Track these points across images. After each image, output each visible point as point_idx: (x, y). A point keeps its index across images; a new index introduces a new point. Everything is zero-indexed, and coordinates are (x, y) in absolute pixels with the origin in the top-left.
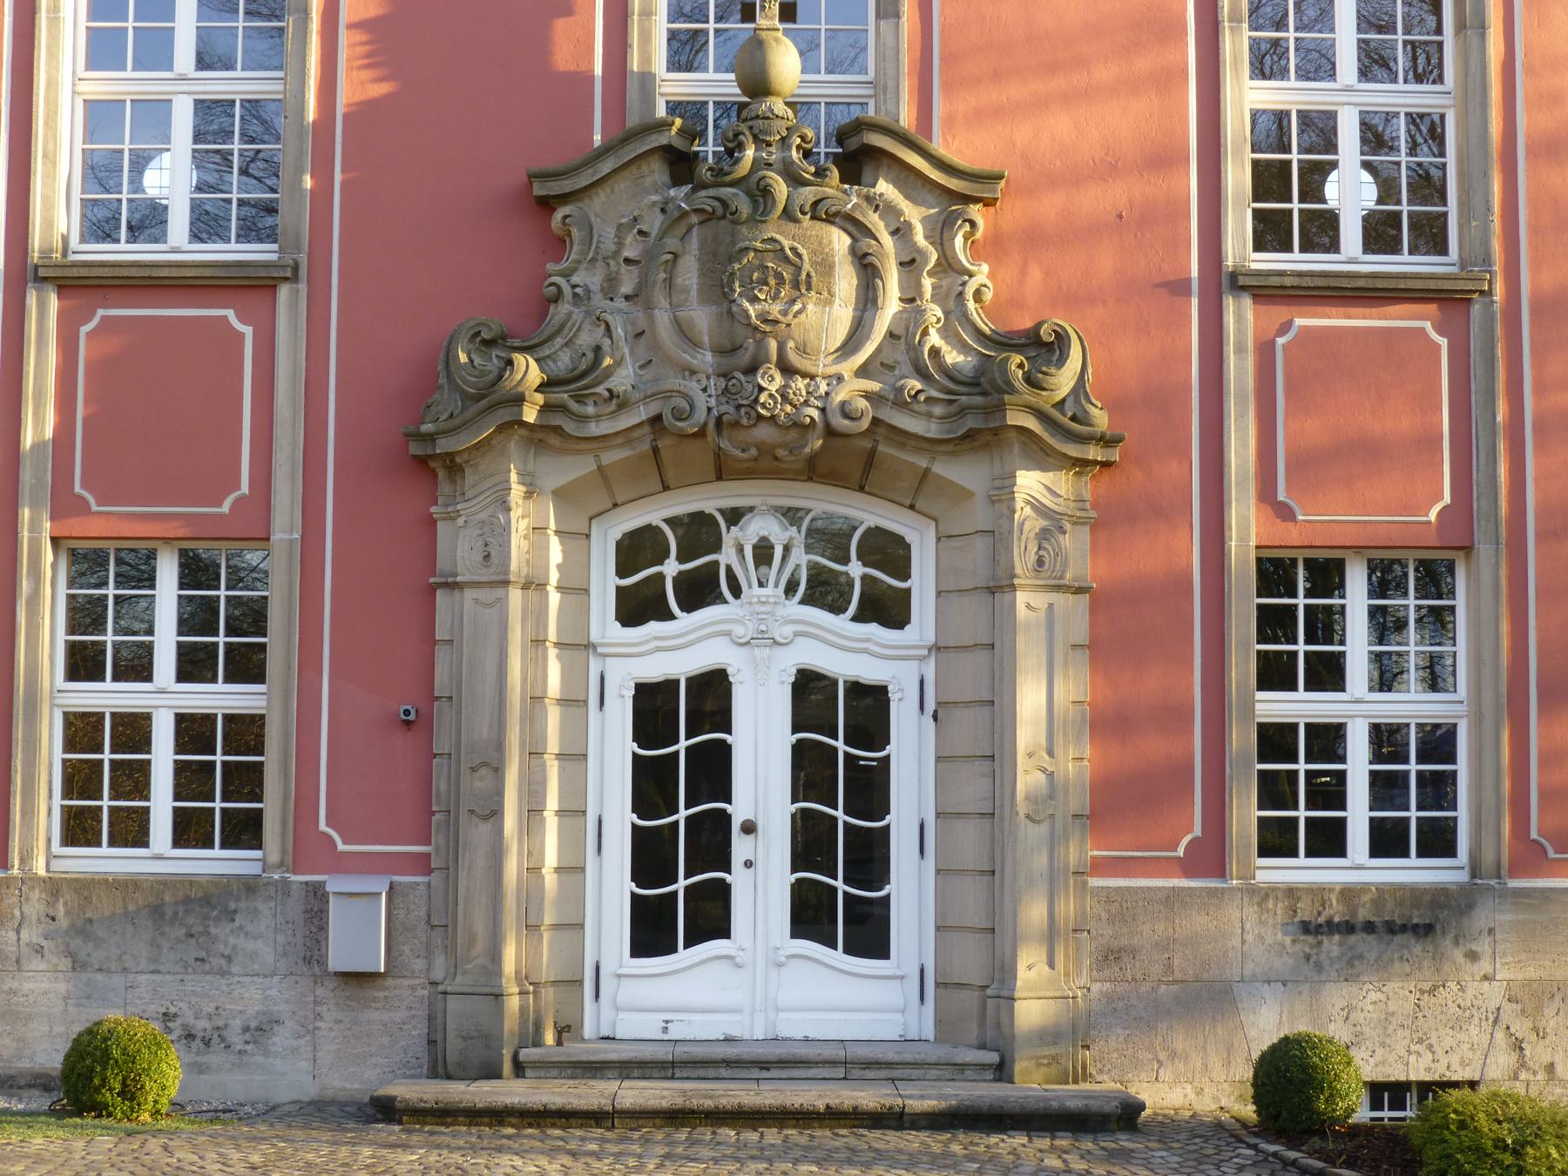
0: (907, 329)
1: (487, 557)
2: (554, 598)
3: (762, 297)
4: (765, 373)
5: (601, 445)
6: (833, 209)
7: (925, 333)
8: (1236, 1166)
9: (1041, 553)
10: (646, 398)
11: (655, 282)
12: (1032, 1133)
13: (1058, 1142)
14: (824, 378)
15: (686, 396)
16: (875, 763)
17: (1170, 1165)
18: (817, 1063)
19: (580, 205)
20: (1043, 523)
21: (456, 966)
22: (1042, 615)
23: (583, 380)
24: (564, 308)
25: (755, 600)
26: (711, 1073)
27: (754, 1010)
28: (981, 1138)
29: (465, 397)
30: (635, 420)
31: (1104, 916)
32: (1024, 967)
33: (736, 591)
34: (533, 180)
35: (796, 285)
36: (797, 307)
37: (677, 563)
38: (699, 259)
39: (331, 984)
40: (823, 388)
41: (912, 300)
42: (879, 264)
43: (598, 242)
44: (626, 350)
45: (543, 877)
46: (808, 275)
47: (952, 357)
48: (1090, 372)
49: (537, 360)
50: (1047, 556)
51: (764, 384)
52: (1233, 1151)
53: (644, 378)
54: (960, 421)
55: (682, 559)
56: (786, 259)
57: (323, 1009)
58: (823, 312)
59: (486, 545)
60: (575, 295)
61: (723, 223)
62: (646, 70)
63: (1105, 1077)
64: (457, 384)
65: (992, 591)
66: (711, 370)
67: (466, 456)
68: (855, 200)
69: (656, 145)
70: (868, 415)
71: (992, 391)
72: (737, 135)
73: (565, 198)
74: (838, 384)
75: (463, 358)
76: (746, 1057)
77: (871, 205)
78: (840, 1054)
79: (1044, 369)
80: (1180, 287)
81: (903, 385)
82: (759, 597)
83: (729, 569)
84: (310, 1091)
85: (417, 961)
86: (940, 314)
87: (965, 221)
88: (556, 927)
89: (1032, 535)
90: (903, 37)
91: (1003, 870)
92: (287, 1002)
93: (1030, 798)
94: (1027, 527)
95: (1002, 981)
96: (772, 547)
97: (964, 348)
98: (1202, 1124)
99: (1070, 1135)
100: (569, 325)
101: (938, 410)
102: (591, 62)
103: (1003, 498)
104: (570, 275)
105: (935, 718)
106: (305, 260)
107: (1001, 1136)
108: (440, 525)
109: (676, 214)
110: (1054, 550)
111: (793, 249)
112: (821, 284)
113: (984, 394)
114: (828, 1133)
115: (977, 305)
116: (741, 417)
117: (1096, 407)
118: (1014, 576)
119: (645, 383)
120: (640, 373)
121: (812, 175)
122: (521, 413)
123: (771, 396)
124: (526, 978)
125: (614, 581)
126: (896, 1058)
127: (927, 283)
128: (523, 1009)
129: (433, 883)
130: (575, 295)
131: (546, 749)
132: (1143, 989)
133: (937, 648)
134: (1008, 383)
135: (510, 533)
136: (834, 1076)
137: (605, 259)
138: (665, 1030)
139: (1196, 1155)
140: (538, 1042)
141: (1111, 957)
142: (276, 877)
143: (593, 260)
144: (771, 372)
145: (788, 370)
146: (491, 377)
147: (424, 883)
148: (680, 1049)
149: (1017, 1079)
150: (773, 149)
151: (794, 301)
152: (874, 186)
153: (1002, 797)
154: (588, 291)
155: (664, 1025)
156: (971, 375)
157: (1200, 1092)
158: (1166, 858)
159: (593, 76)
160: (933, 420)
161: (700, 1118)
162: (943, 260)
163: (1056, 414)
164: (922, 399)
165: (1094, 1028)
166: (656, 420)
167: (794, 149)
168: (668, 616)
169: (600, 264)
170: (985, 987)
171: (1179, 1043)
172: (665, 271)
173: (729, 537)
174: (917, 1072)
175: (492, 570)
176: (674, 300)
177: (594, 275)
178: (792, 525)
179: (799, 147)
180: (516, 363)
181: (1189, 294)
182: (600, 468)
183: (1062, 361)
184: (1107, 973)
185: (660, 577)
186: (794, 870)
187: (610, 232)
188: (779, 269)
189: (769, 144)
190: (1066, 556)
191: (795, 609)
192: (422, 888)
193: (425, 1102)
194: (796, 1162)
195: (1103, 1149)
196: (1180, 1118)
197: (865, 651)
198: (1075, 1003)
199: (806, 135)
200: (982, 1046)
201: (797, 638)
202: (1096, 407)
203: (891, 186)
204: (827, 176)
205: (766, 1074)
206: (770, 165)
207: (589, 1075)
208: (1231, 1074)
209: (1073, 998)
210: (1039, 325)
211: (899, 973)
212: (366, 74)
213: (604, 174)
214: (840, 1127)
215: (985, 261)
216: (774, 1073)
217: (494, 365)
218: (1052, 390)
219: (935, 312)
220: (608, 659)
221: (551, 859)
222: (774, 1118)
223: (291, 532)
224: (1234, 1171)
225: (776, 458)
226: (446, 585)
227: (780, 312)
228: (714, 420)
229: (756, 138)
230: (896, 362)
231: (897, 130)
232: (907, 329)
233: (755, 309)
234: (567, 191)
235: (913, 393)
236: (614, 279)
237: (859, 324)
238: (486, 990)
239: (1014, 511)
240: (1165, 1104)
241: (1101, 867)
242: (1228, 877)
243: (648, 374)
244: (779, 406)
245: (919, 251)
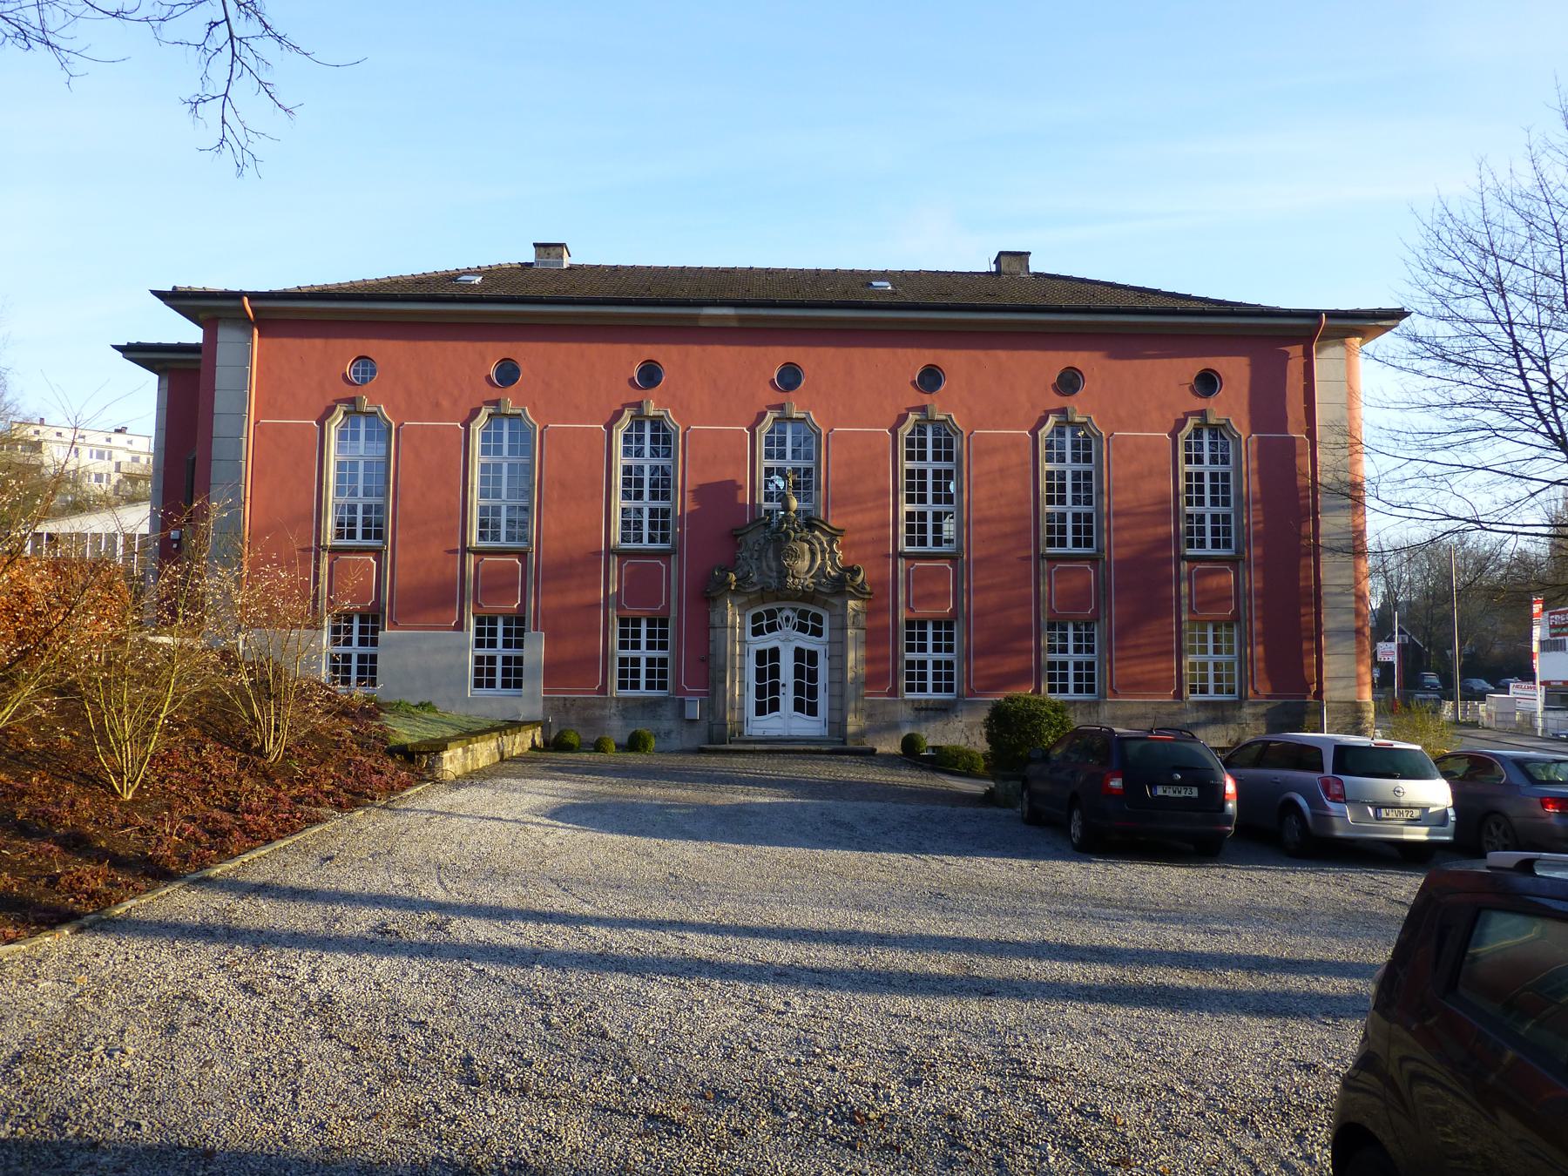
47: (833, 573)
73: (741, 535)
80: (887, 556)
125: (751, 626)
145: (794, 577)
166: (762, 589)
171: (886, 736)
173: (779, 615)
221: (737, 692)
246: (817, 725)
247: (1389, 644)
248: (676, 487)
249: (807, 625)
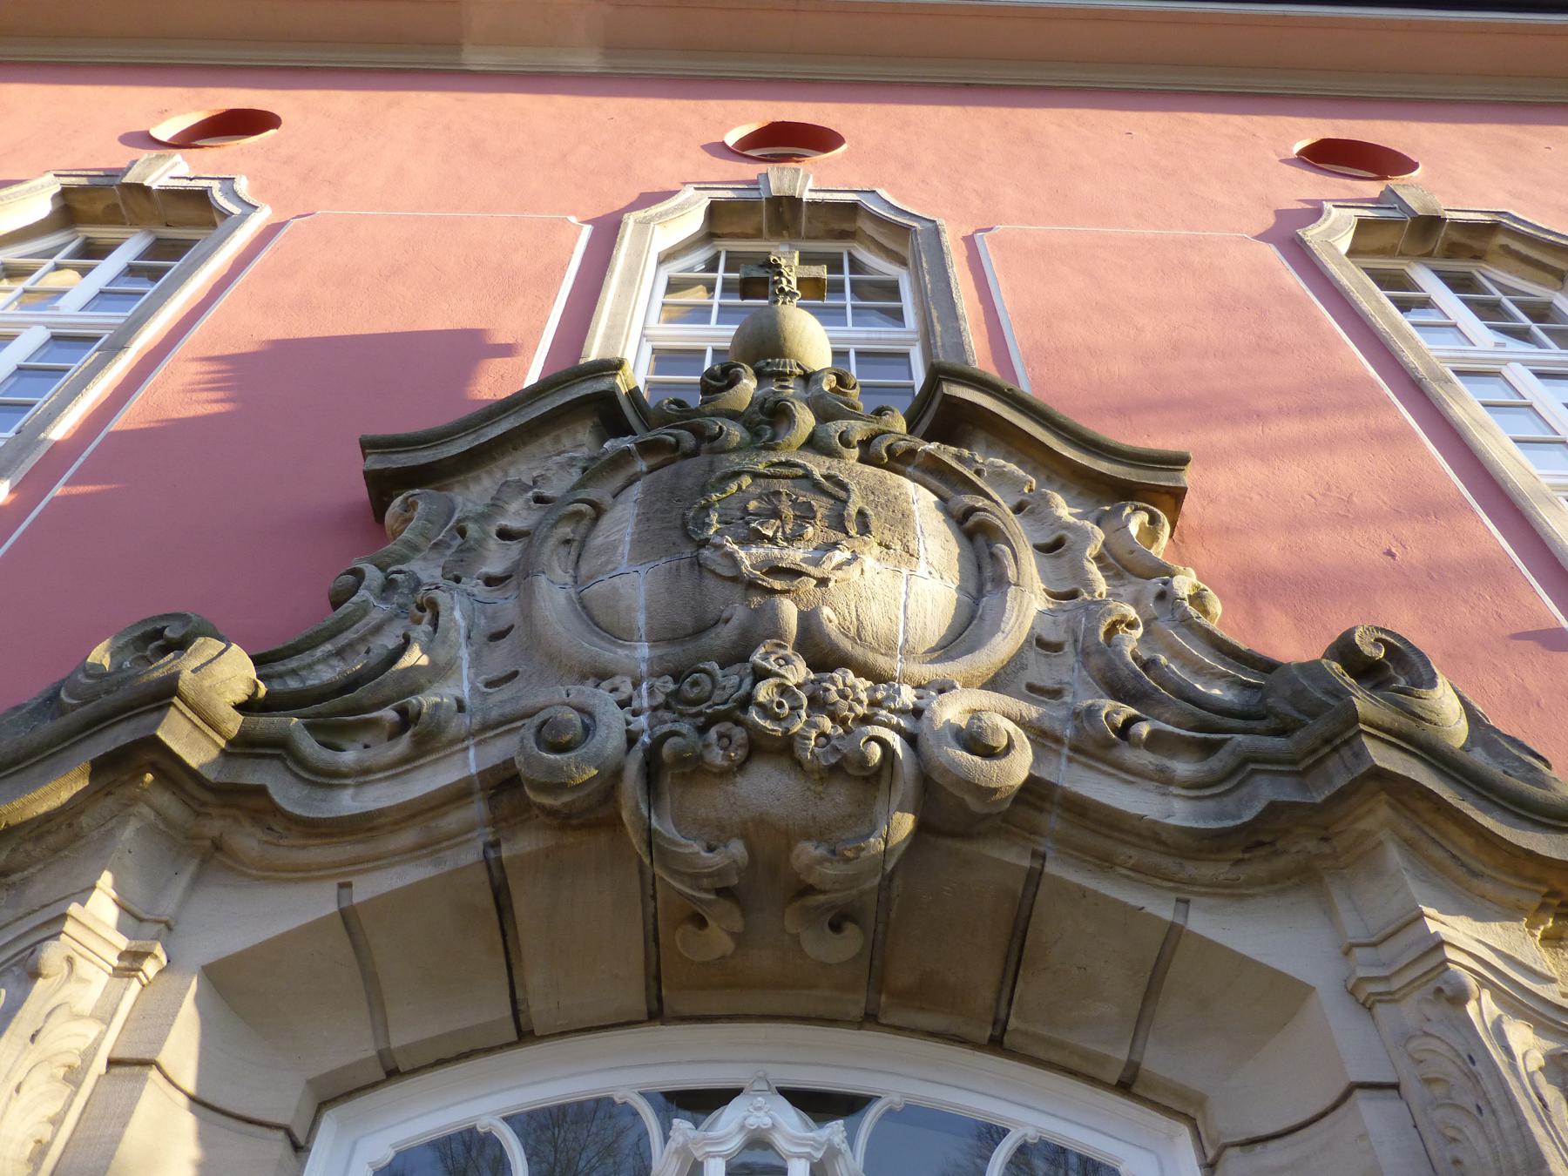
35: (839, 523)
54: (1244, 791)
66: (644, 667)
103: (1396, 984)
116: (707, 746)
123: (784, 690)
237: (972, 618)
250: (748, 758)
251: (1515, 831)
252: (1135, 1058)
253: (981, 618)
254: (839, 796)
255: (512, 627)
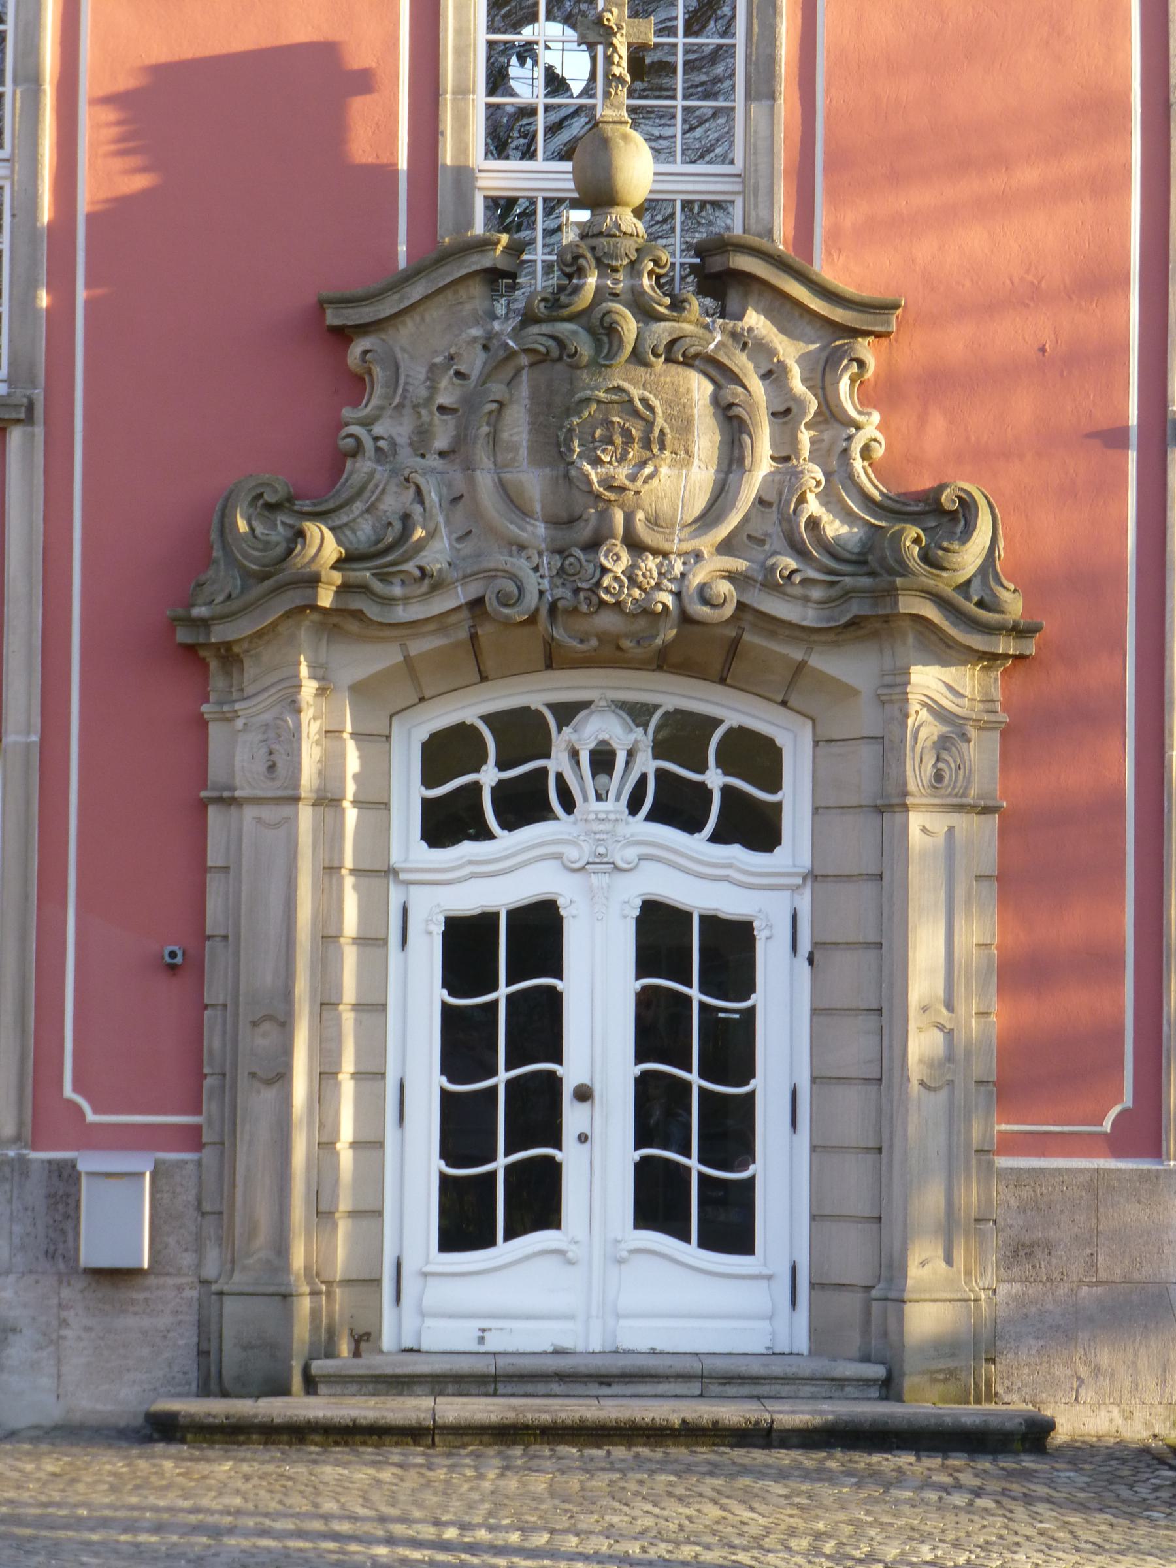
0: (780, 494)
1: (272, 768)
2: (351, 815)
3: (607, 459)
4: (609, 551)
5: (409, 631)
6: (692, 351)
7: (802, 500)
8: (1151, 1487)
9: (940, 765)
10: (465, 577)
11: (476, 437)
12: (921, 1453)
13: (950, 1462)
14: (679, 555)
15: (513, 577)
16: (737, 1016)
17: (1077, 1485)
18: (668, 1377)
19: (383, 336)
20: (944, 729)
21: (233, 1262)
22: (941, 840)
23: (385, 557)
24: (364, 466)
25: (592, 816)
26: (541, 1388)
27: (589, 1317)
28: (861, 1457)
29: (246, 574)
30: (451, 604)
31: (1014, 1203)
32: (916, 1262)
33: (569, 805)
34: (325, 306)
35: (647, 444)
36: (648, 470)
37: (496, 770)
38: (530, 411)
39: (79, 1283)
40: (678, 568)
41: (787, 459)
42: (746, 417)
43: (406, 383)
44: (441, 519)
45: (337, 1154)
46: (662, 432)
47: (834, 528)
48: (1001, 546)
49: (332, 529)
50: (946, 769)
51: (607, 564)
52: (1153, 1472)
53: (462, 553)
55: (502, 766)
56: (636, 413)
57: (69, 1315)
58: (679, 476)
59: (271, 753)
60: (378, 450)
61: (559, 366)
62: (462, 164)
63: (1015, 1397)
64: (236, 560)
65: (880, 810)
66: (543, 546)
67: (246, 645)
68: (718, 338)
69: (478, 267)
70: (732, 600)
71: (882, 572)
72: (576, 258)
73: (364, 329)
74: (696, 563)
75: (242, 526)
76: (583, 1369)
77: (738, 342)
78: (696, 1367)
79: (945, 544)
80: (1116, 438)
81: (774, 564)
82: (596, 813)
83: (560, 777)
84: (54, 1413)
85: (185, 1255)
86: (820, 476)
87: (852, 360)
88: (354, 1214)
89: (929, 744)
90: (779, 124)
91: (891, 1146)
92: (25, 1306)
93: (931, 1064)
94: (922, 735)
95: (890, 1280)
96: (613, 753)
97: (848, 516)
98: (1126, 1448)
99: (966, 1455)
100: (371, 486)
101: (816, 593)
102: (394, 152)
104: (372, 424)
105: (811, 961)
106: (42, 397)
107: (885, 1456)
108: (213, 728)
109: (502, 354)
110: (955, 762)
111: (644, 400)
112: (676, 442)
113: (872, 574)
114: (683, 1450)
115: (866, 463)
117: (1008, 589)
118: (906, 794)
119: (464, 559)
120: (458, 546)
121: (667, 307)
122: (315, 597)
123: (616, 578)
124: (318, 1275)
125: (420, 792)
126: (763, 1372)
127: (805, 437)
128: (315, 1314)
129: (204, 1161)
130: (378, 450)
131: (342, 999)
132: (1060, 1292)
133: (813, 876)
134: (902, 562)
135: (300, 739)
136: (689, 1393)
137: (415, 407)
138: (481, 1340)
139: (1109, 1476)
140: (330, 1354)
141: (1022, 1253)
142: (11, 1153)
143: (400, 406)
144: (617, 549)
145: (636, 546)
146: (280, 550)
147: (192, 1161)
148: (502, 1362)
149: (906, 1397)
150: (620, 276)
151: (643, 464)
152: (740, 317)
153: (891, 1059)
154: (393, 444)
155: (480, 1334)
156: (856, 550)
157: (1128, 1416)
158: (1090, 1134)
159: (397, 171)
160: (810, 604)
161: (535, 1435)
162: (824, 409)
163: (958, 599)
164: (798, 581)
165: (1002, 1338)
166: (477, 604)
167: (646, 275)
168: (486, 834)
169: (408, 411)
170: (868, 1289)
171: (1104, 1357)
172: (488, 424)
173: (560, 741)
174: (787, 1388)
175: (278, 783)
176: (500, 458)
177: (401, 424)
178: (638, 725)
179: (651, 273)
180: (308, 535)
181: (1125, 446)
182: (407, 658)
183: (967, 533)
184: (1016, 1272)
185: (476, 787)
186: (751, 1096)
187: (421, 372)
188: (627, 425)
189: (615, 270)
190: (970, 770)
191: (641, 827)
192: (191, 1167)
193: (214, 1417)
194: (652, 1472)
195: (1003, 1469)
196: (1101, 1444)
197: (726, 879)
198: (978, 1308)
199: (660, 259)
200: (866, 1359)
201: (642, 863)
202: (1008, 589)
203: (762, 317)
204: (684, 309)
205: (606, 1390)
206: (616, 295)
207: (394, 1391)
208: (1167, 1395)
209: (976, 1301)
210: (941, 488)
211: (766, 1271)
212: (118, 164)
213: (412, 301)
214: (698, 1445)
215: (875, 407)
216: (616, 1389)
217: (279, 534)
218: (955, 570)
219: (814, 473)
220: (413, 888)
221: (347, 1132)
222: (620, 1435)
223: (28, 734)
224: (1149, 1491)
225: (619, 648)
226: (220, 800)
227: (627, 477)
228: (547, 606)
229: (599, 262)
230: (767, 535)
231: (771, 251)
232: (780, 494)
233: (597, 473)
234: (368, 320)
235: (786, 573)
236: (426, 431)
238: (272, 1289)
239: (907, 716)
240: (1086, 1429)
241: (1012, 1145)
242: (1164, 1157)
243: (467, 548)
244: (626, 590)
245: (796, 399)
246: (756, 1297)
247: (624, 567)
248: (31, 79)
249: (703, 792)
250: (599, 608)
251: (968, 636)
252: (786, 699)
253: (727, 491)
254: (642, 622)
255: (462, 496)
